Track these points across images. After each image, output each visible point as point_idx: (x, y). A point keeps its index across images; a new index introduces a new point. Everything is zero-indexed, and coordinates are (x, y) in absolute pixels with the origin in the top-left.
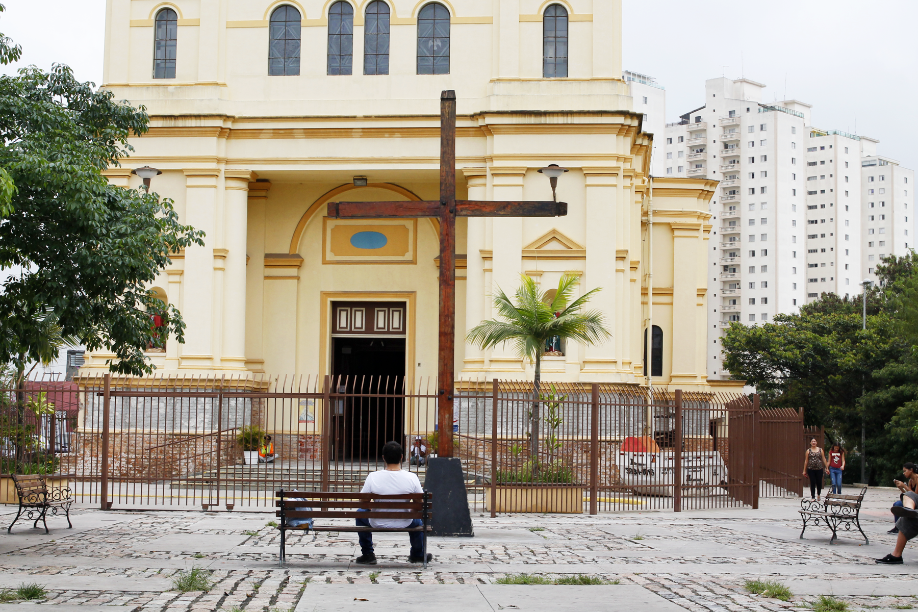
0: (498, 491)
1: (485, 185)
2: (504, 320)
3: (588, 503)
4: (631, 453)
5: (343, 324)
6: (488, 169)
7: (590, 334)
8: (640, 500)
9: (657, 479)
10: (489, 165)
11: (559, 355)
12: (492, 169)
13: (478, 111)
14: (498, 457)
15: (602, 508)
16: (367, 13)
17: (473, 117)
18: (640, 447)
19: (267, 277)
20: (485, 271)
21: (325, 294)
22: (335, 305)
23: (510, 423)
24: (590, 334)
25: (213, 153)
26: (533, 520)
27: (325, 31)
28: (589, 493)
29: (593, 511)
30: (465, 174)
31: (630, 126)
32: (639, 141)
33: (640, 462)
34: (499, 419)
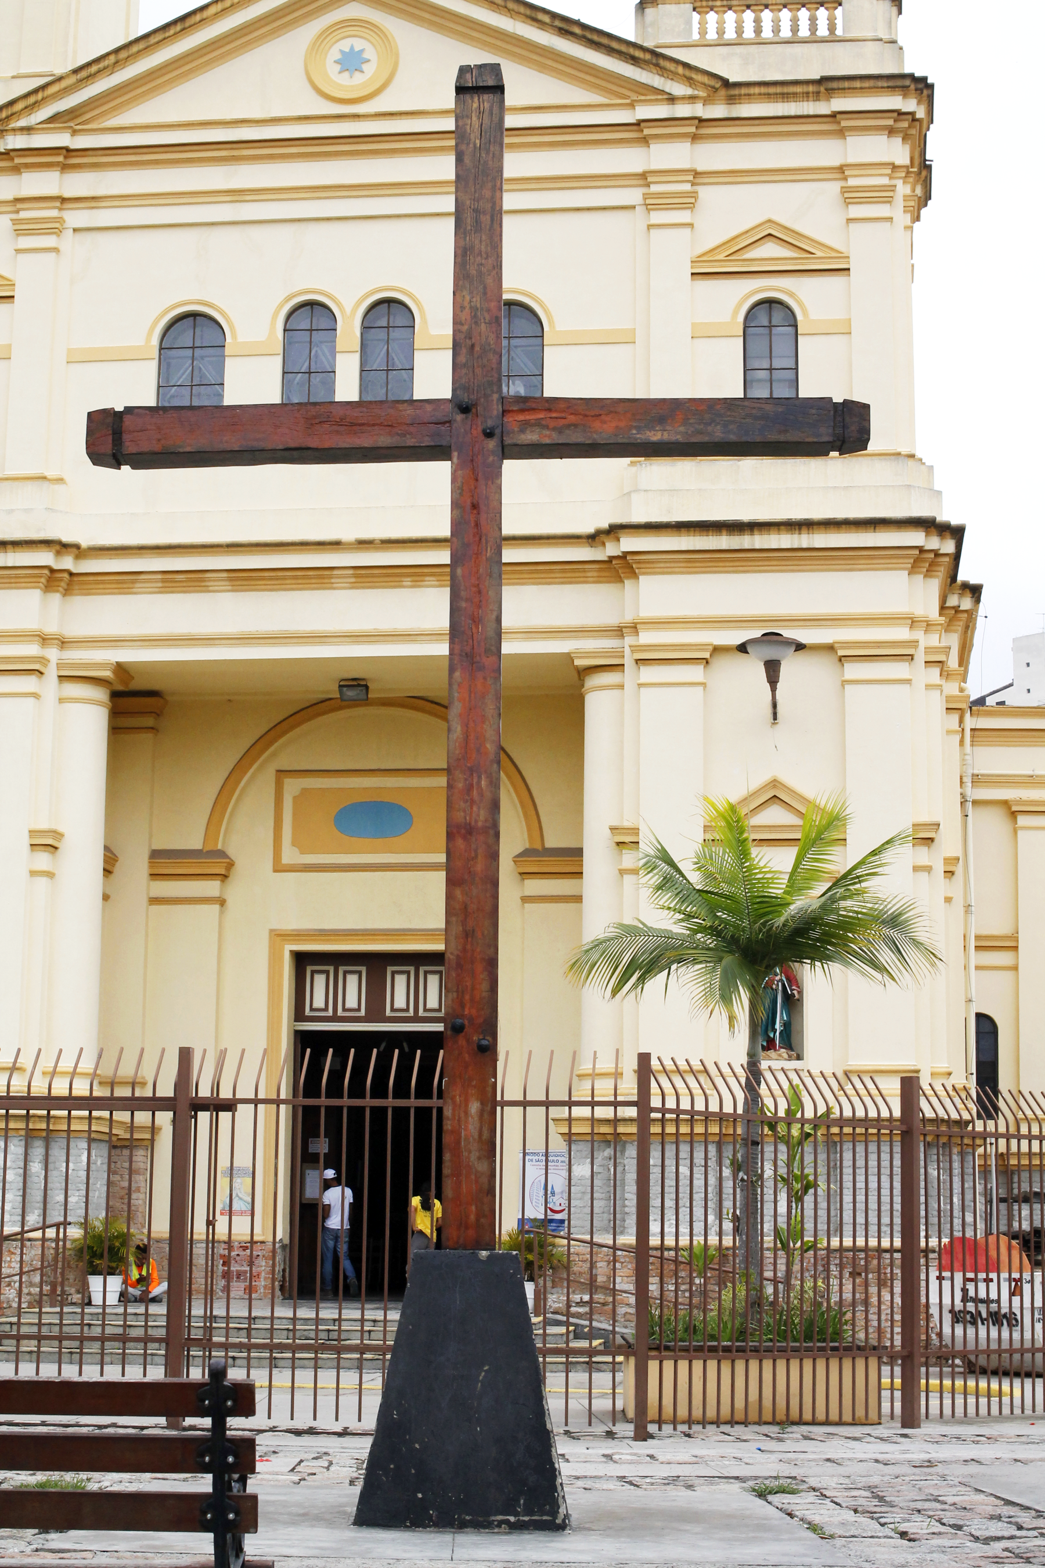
0: (653, 1366)
1: (621, 687)
2: (663, 919)
3: (898, 1394)
4: (958, 1277)
5: (319, 1002)
6: (627, 650)
7: (886, 956)
8: (1006, 1388)
9: (1028, 1335)
10: (629, 640)
11: (790, 1058)
12: (634, 649)
13: (605, 525)
14: (654, 1288)
15: (934, 1410)
16: (365, 328)
17: (594, 538)
18: (982, 1260)
19: (154, 901)
20: (622, 872)
21: (278, 936)
22: (302, 961)
23: (684, 1212)
24: (886, 956)
25: (31, 623)
26: (758, 1455)
27: (276, 364)
28: (898, 1370)
29: (910, 1419)
30: (578, 662)
31: (937, 554)
32: (953, 601)
33: (982, 1294)
34: (655, 1202)
